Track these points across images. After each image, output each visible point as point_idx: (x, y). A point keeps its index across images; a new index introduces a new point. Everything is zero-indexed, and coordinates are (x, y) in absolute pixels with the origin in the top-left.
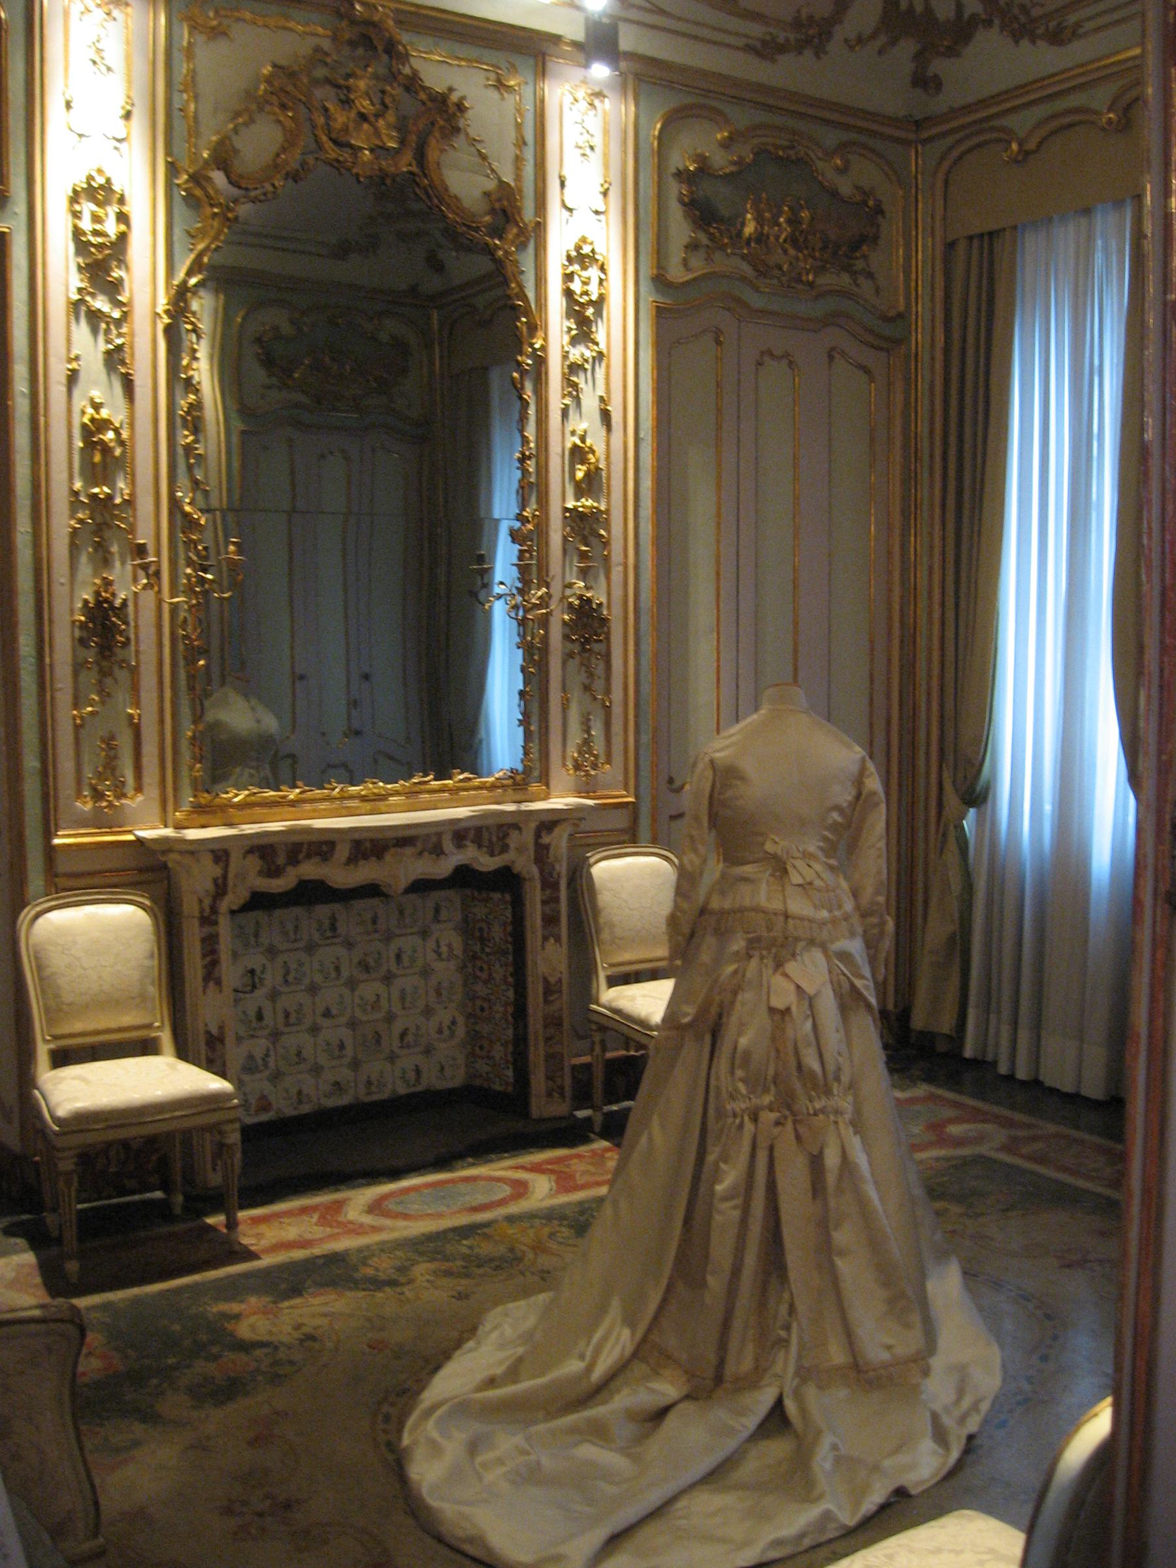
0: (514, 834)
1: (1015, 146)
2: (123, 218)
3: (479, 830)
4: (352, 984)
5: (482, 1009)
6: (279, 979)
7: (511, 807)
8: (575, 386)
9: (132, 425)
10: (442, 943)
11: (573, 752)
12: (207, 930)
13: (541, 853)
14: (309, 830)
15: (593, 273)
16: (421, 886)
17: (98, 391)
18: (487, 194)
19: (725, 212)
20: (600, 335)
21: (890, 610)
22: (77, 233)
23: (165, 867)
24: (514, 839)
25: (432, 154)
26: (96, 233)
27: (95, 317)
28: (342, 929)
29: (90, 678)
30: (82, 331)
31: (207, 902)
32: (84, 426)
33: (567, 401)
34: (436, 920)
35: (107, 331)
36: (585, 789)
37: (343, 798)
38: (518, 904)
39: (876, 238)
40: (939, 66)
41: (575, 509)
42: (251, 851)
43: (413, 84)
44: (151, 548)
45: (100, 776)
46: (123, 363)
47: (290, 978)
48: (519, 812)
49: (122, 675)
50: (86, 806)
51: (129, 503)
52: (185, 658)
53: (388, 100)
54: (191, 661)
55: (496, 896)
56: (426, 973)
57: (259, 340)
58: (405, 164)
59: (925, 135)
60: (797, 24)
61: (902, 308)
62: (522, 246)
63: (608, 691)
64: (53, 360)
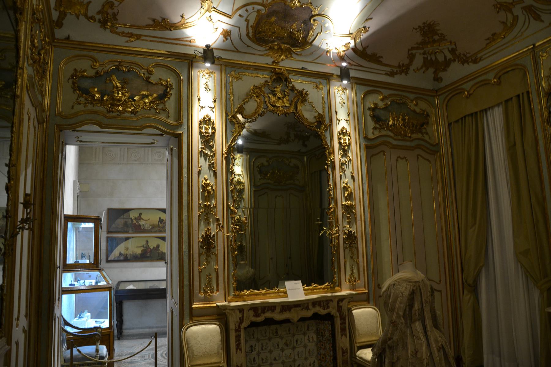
0: (331, 303)
1: (466, 93)
2: (213, 128)
3: (320, 302)
4: (283, 350)
5: (323, 358)
6: (260, 349)
7: (329, 295)
8: (343, 169)
9: (216, 185)
10: (310, 337)
11: (348, 277)
12: (237, 333)
13: (340, 309)
14: (268, 303)
15: (347, 137)
16: (303, 319)
17: (206, 175)
18: (315, 117)
19: (383, 118)
20: (350, 155)
21: (442, 229)
22: (201, 133)
23: (225, 314)
24: (331, 304)
25: (299, 107)
26: (206, 133)
27: (206, 155)
28: (279, 333)
29: (203, 257)
30: (202, 159)
31: (237, 325)
32: (202, 185)
33: (341, 173)
34: (308, 329)
35: (209, 159)
36: (353, 288)
37: (278, 293)
38: (333, 325)
39: (427, 123)
40: (441, 74)
41: (345, 204)
42: (250, 309)
43: (293, 89)
44: (221, 220)
45: (207, 287)
46: (214, 167)
47: (264, 348)
48: (332, 296)
49: (213, 257)
50: (202, 295)
51: (215, 207)
52: (231, 252)
53: (286, 93)
54: (233, 252)
55: (326, 322)
56: (305, 346)
57: (258, 167)
58: (292, 109)
59: (439, 94)
60: (399, 66)
61: (437, 142)
62: (326, 130)
63: (358, 258)
64: (194, 167)
